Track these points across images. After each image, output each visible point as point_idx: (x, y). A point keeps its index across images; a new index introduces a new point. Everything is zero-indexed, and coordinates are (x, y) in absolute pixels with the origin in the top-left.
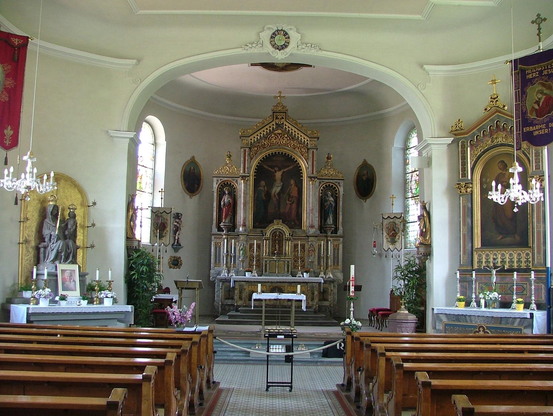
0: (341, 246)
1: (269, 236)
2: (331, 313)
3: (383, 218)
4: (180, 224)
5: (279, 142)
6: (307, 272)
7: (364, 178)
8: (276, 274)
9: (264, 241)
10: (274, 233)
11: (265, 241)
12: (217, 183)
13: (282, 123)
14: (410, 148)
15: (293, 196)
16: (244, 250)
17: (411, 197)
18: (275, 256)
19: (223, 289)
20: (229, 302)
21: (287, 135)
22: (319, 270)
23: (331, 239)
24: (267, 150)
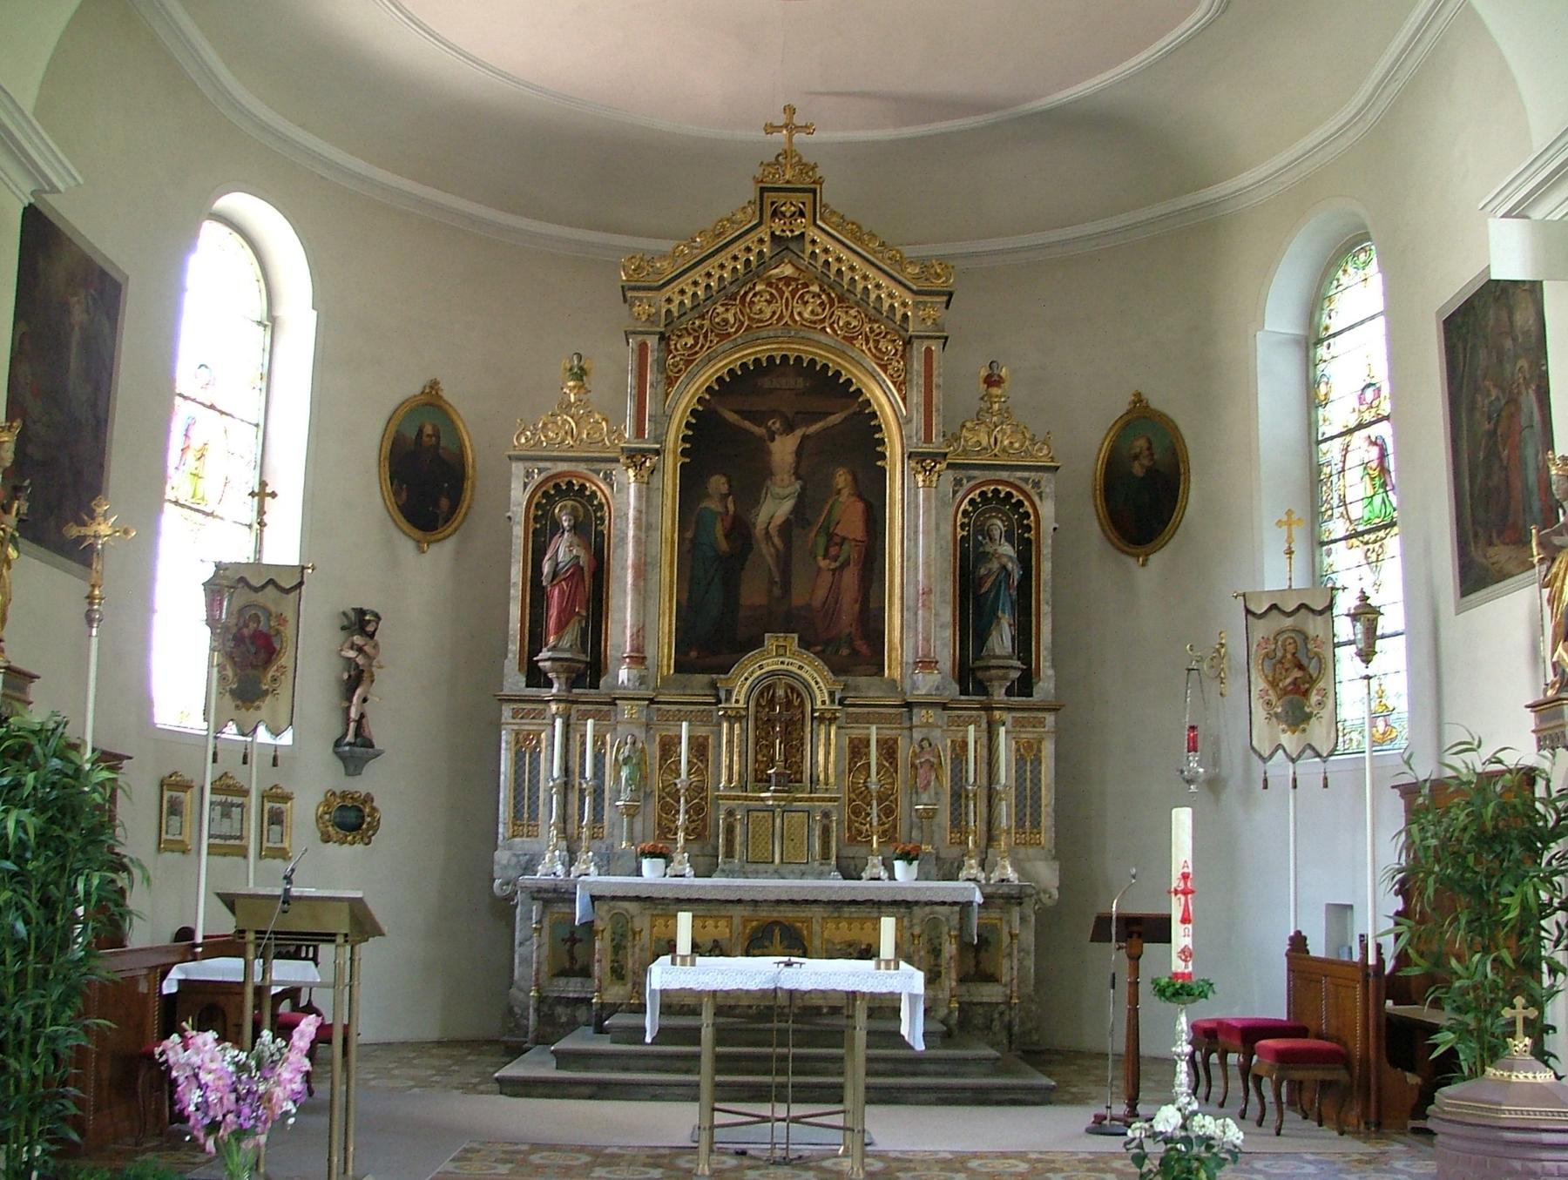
0: (1048, 749)
1: (742, 704)
2: (1010, 1035)
3: (1248, 611)
4: (369, 658)
5: (787, 314)
6: (908, 857)
7: (1138, 469)
8: (771, 866)
9: (720, 725)
10: (765, 693)
11: (725, 725)
12: (525, 485)
13: (797, 233)
14: (1334, 335)
15: (844, 539)
16: (637, 761)
17: (1346, 538)
18: (768, 790)
19: (546, 932)
20: (572, 988)
21: (821, 287)
22: (956, 851)
23: (1008, 717)
24: (736, 348)
